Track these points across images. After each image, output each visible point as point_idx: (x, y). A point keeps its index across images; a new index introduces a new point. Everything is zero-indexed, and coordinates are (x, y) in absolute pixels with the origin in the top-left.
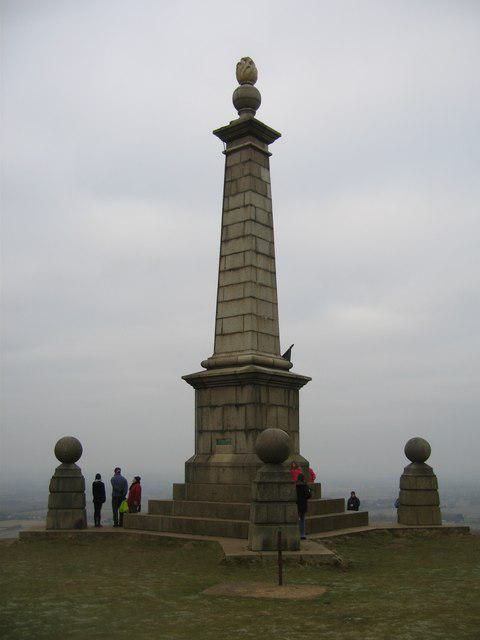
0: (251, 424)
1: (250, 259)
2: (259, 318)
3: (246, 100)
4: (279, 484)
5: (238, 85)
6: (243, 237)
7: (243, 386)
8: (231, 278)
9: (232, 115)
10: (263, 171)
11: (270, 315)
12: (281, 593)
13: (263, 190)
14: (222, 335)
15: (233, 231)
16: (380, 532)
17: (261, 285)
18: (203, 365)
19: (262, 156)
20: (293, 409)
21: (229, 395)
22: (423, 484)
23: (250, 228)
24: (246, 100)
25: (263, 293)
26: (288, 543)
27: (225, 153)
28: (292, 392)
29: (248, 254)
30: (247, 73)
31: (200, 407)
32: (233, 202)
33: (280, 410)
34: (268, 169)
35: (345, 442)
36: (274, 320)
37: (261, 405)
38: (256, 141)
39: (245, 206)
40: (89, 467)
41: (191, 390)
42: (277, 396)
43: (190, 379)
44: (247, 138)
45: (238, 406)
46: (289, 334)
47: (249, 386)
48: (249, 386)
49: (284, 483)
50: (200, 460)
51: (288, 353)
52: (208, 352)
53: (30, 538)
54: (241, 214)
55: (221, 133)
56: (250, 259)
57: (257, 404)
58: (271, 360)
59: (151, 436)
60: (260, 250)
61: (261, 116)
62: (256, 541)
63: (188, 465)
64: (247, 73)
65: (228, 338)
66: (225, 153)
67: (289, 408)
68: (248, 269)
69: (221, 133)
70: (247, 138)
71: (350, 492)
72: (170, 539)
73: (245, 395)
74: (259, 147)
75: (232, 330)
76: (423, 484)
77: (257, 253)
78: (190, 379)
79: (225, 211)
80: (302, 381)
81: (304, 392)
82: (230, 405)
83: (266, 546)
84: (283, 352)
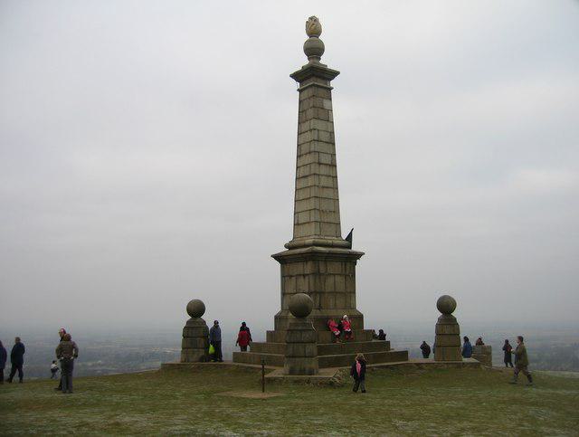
0: (312, 290)
1: (315, 169)
2: (321, 211)
3: (314, 50)
4: (300, 331)
5: (307, 38)
6: (310, 153)
7: (307, 262)
8: (303, 183)
9: (303, 61)
10: (326, 103)
11: (332, 209)
12: (266, 396)
13: (326, 116)
14: (298, 224)
15: (305, 148)
16: (410, 366)
17: (323, 187)
18: (286, 246)
19: (325, 91)
20: (351, 276)
21: (299, 268)
22: (447, 330)
23: (318, 146)
24: (314, 50)
25: (327, 193)
26: (307, 369)
27: (298, 90)
28: (348, 264)
29: (313, 166)
30: (313, 28)
31: (285, 276)
32: (306, 126)
33: (338, 279)
34: (331, 99)
35: (390, 301)
36: (336, 212)
37: (320, 274)
38: (319, 80)
39: (311, 130)
40: (209, 319)
41: (278, 265)
42: (335, 267)
43: (277, 257)
44: (315, 79)
45: (304, 276)
46: (349, 219)
47: (319, 262)
48: (319, 262)
49: (304, 330)
50: (283, 314)
51: (350, 237)
52: (289, 238)
53: (169, 369)
54: (308, 136)
55: (296, 76)
56: (315, 169)
57: (317, 274)
58: (330, 242)
59: (251, 301)
60: (323, 161)
61: (326, 60)
62: (286, 368)
63: (276, 317)
64: (313, 28)
65: (301, 226)
66: (298, 90)
67: (346, 276)
68: (313, 177)
69: (296, 76)
70: (315, 79)
71: (58, 329)
72: (252, 368)
73: (308, 268)
74: (321, 85)
75: (303, 221)
76: (447, 330)
77: (320, 164)
78: (277, 257)
79: (299, 134)
80: (359, 255)
81: (360, 265)
82: (300, 275)
83: (292, 372)
84: (344, 236)
